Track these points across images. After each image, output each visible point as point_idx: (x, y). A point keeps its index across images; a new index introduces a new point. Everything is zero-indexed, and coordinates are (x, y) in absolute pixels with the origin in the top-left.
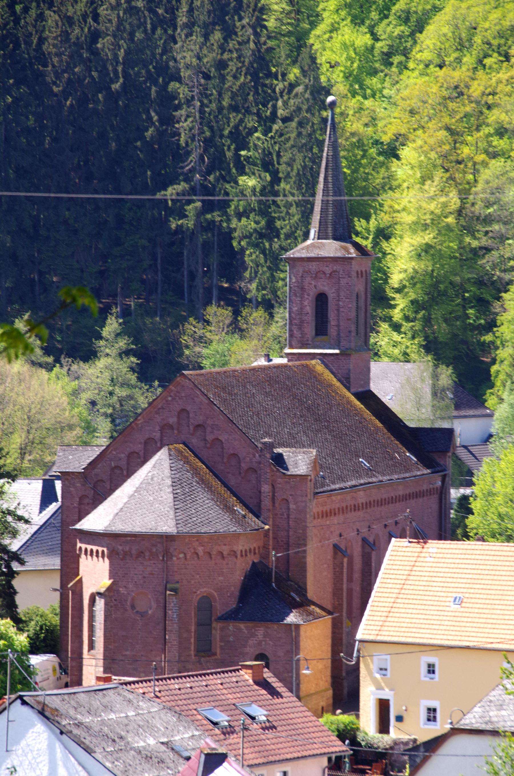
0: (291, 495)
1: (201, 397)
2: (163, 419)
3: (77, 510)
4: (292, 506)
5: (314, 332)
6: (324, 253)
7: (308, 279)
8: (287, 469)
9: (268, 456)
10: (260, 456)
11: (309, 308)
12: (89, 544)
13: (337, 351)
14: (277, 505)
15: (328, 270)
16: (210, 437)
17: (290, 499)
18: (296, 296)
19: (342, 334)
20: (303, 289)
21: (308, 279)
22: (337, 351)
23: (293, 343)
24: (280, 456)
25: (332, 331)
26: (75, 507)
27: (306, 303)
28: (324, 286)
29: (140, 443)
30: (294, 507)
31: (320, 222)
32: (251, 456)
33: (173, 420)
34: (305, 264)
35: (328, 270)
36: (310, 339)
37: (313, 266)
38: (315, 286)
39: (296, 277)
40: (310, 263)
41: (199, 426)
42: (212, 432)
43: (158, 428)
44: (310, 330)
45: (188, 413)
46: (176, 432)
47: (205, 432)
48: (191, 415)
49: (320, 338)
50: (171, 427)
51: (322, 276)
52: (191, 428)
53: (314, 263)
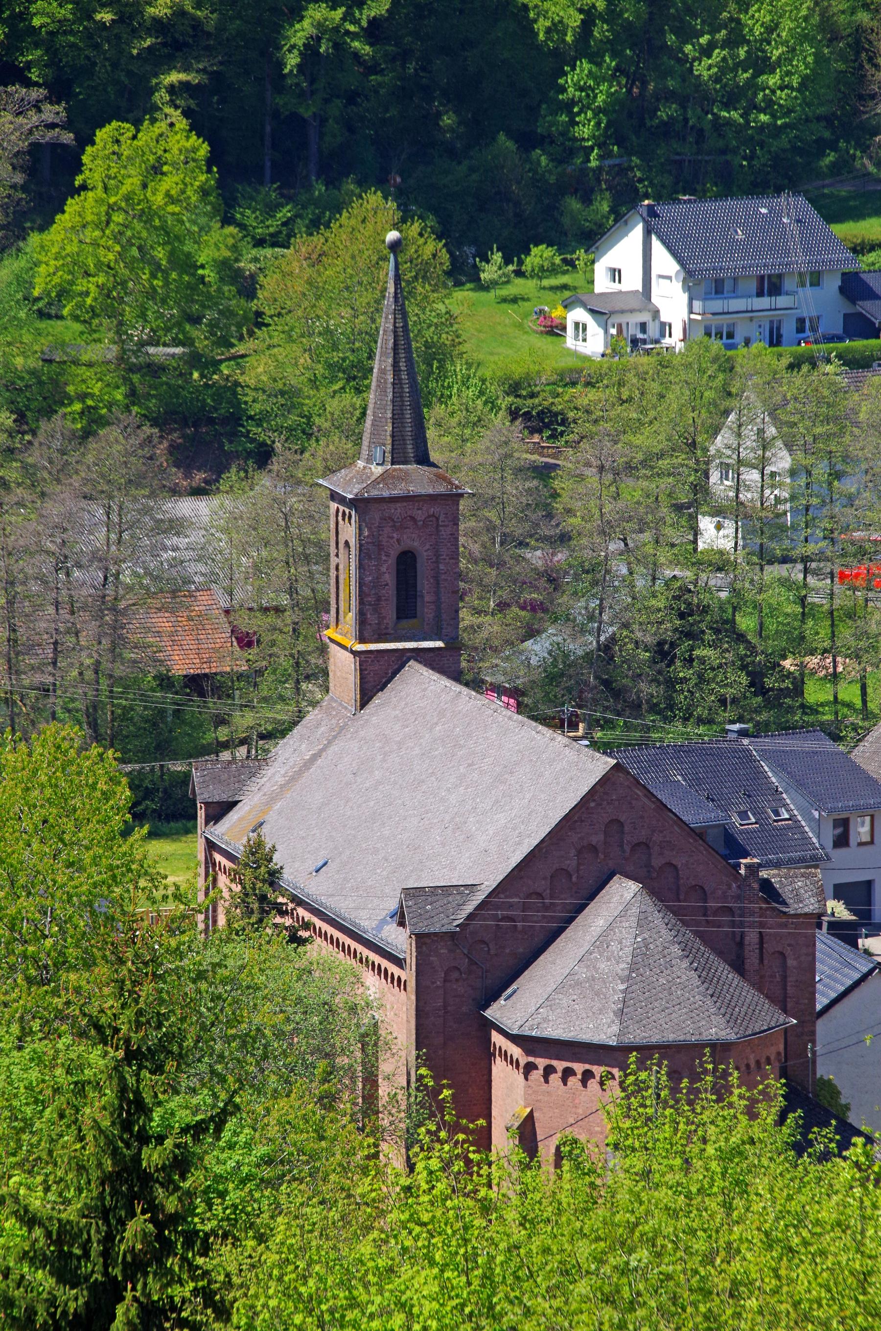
0: (789, 945)
1: (645, 800)
2: (582, 838)
3: (441, 992)
4: (791, 962)
5: (395, 616)
6: (413, 489)
7: (387, 530)
8: (784, 903)
9: (756, 886)
10: (739, 887)
11: (389, 578)
12: (559, 1058)
13: (439, 644)
14: (766, 962)
15: (420, 515)
16: (657, 862)
17: (788, 951)
18: (370, 558)
19: (444, 616)
20: (380, 547)
21: (387, 530)
22: (439, 644)
23: (366, 635)
24: (766, 885)
25: (427, 611)
26: (437, 987)
27: (384, 569)
28: (412, 540)
29: (545, 878)
30: (795, 963)
31: (393, 436)
32: (725, 887)
33: (597, 839)
34: (385, 506)
35: (420, 515)
36: (391, 625)
37: (397, 511)
38: (398, 541)
39: (370, 529)
40: (392, 505)
41: (638, 844)
42: (661, 854)
43: (573, 852)
44: (390, 611)
45: (622, 825)
46: (602, 856)
47: (650, 855)
48: (626, 829)
49: (405, 623)
50: (594, 849)
51: (410, 523)
52: (627, 848)
53: (398, 505)
